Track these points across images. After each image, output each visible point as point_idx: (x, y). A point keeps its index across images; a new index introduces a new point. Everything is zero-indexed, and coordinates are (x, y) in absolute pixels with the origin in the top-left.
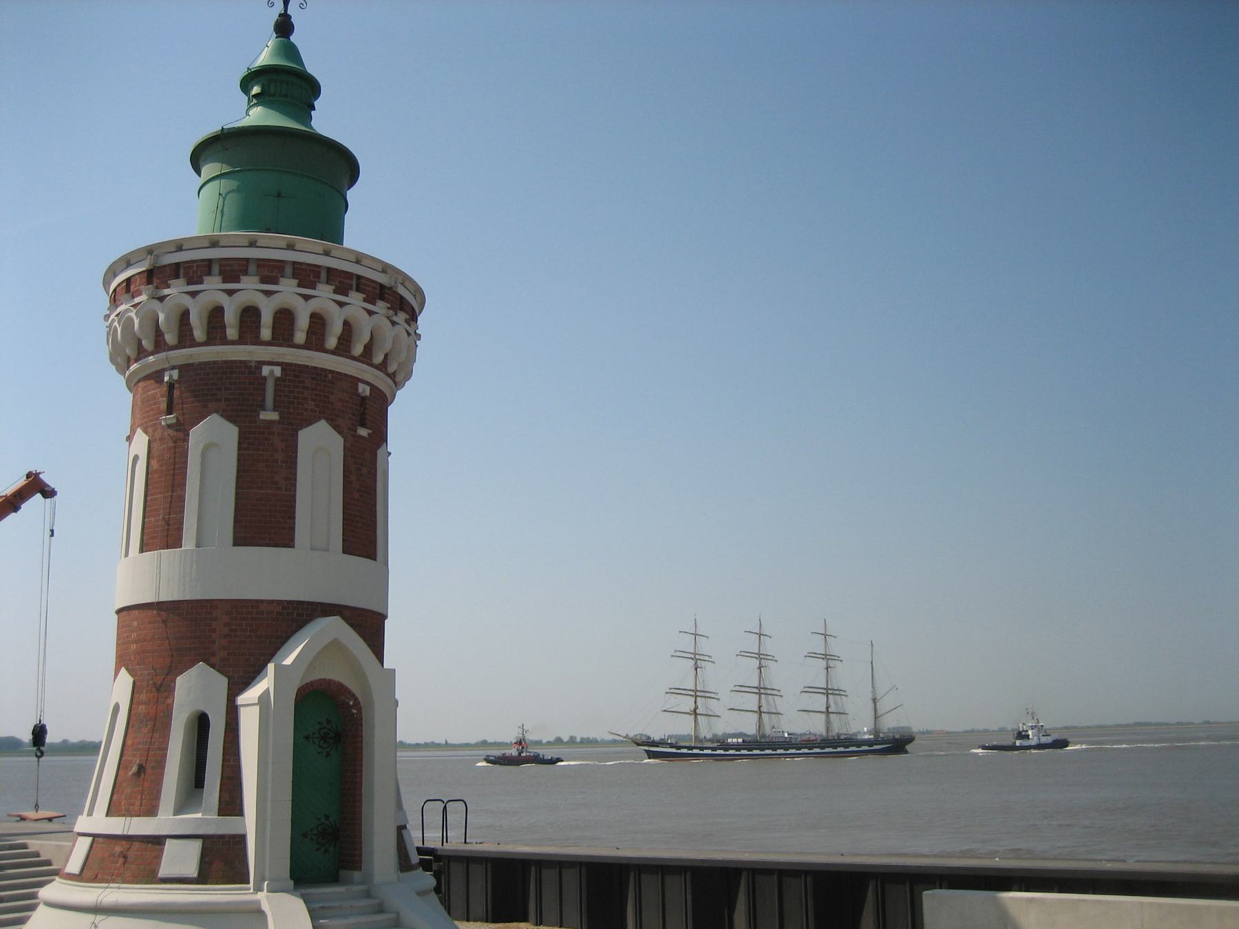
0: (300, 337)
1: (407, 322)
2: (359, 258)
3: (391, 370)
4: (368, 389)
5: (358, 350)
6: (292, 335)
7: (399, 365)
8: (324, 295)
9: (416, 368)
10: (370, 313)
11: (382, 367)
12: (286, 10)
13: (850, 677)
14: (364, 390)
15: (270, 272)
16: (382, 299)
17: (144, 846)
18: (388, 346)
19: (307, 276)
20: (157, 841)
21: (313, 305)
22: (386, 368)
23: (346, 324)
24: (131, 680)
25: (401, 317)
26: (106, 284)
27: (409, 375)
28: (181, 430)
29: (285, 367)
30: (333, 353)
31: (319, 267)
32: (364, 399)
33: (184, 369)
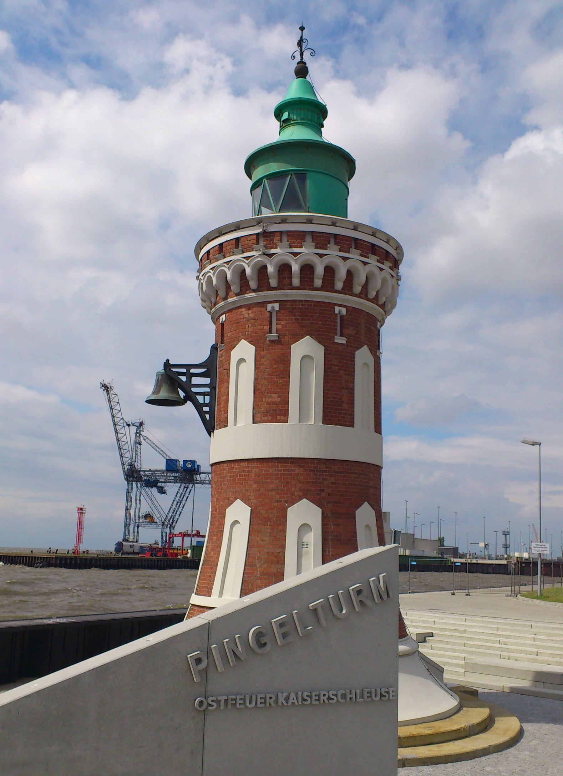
0: (318, 283)
2: (356, 227)
3: (381, 301)
5: (358, 289)
6: (312, 282)
9: (399, 301)
10: (365, 263)
11: (375, 300)
12: (302, 58)
13: (410, 525)
15: (297, 238)
19: (321, 240)
21: (326, 261)
23: (350, 273)
25: (386, 266)
26: (197, 255)
27: (394, 306)
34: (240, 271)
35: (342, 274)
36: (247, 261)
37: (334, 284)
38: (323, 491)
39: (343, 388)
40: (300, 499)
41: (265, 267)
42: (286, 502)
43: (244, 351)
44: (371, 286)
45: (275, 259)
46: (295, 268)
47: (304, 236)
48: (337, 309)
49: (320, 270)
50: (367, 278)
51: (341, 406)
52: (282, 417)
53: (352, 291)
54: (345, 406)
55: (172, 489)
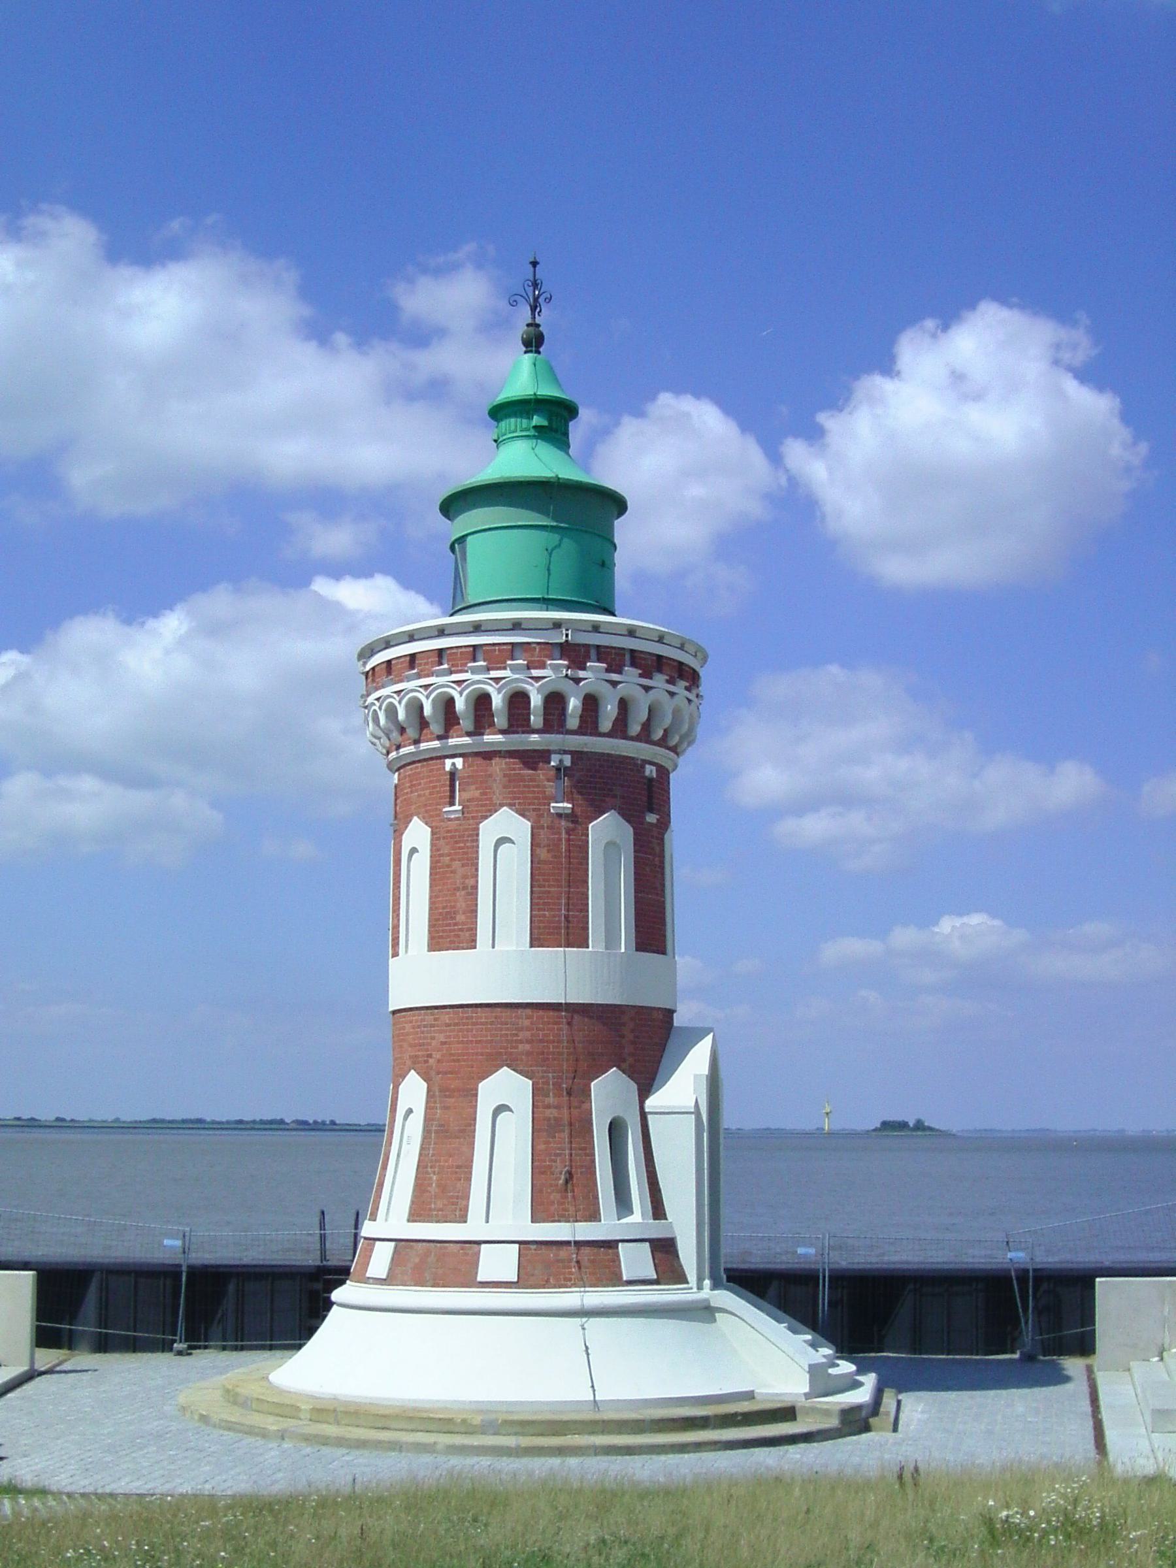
3: (672, 743)
4: (654, 768)
5: (635, 729)
8: (593, 674)
10: (647, 689)
11: (663, 743)
14: (650, 771)
16: (660, 671)
17: (596, 1250)
18: (667, 722)
20: (611, 1245)
23: (623, 705)
24: (424, 1085)
25: (680, 687)
28: (577, 822)
30: (608, 735)
31: (623, 649)
32: (651, 780)
33: (577, 755)
35: (610, 710)
36: (422, 690)
38: (430, 1056)
39: (457, 889)
46: (536, 700)
50: (650, 710)
51: (454, 918)
53: (625, 731)
54: (460, 918)
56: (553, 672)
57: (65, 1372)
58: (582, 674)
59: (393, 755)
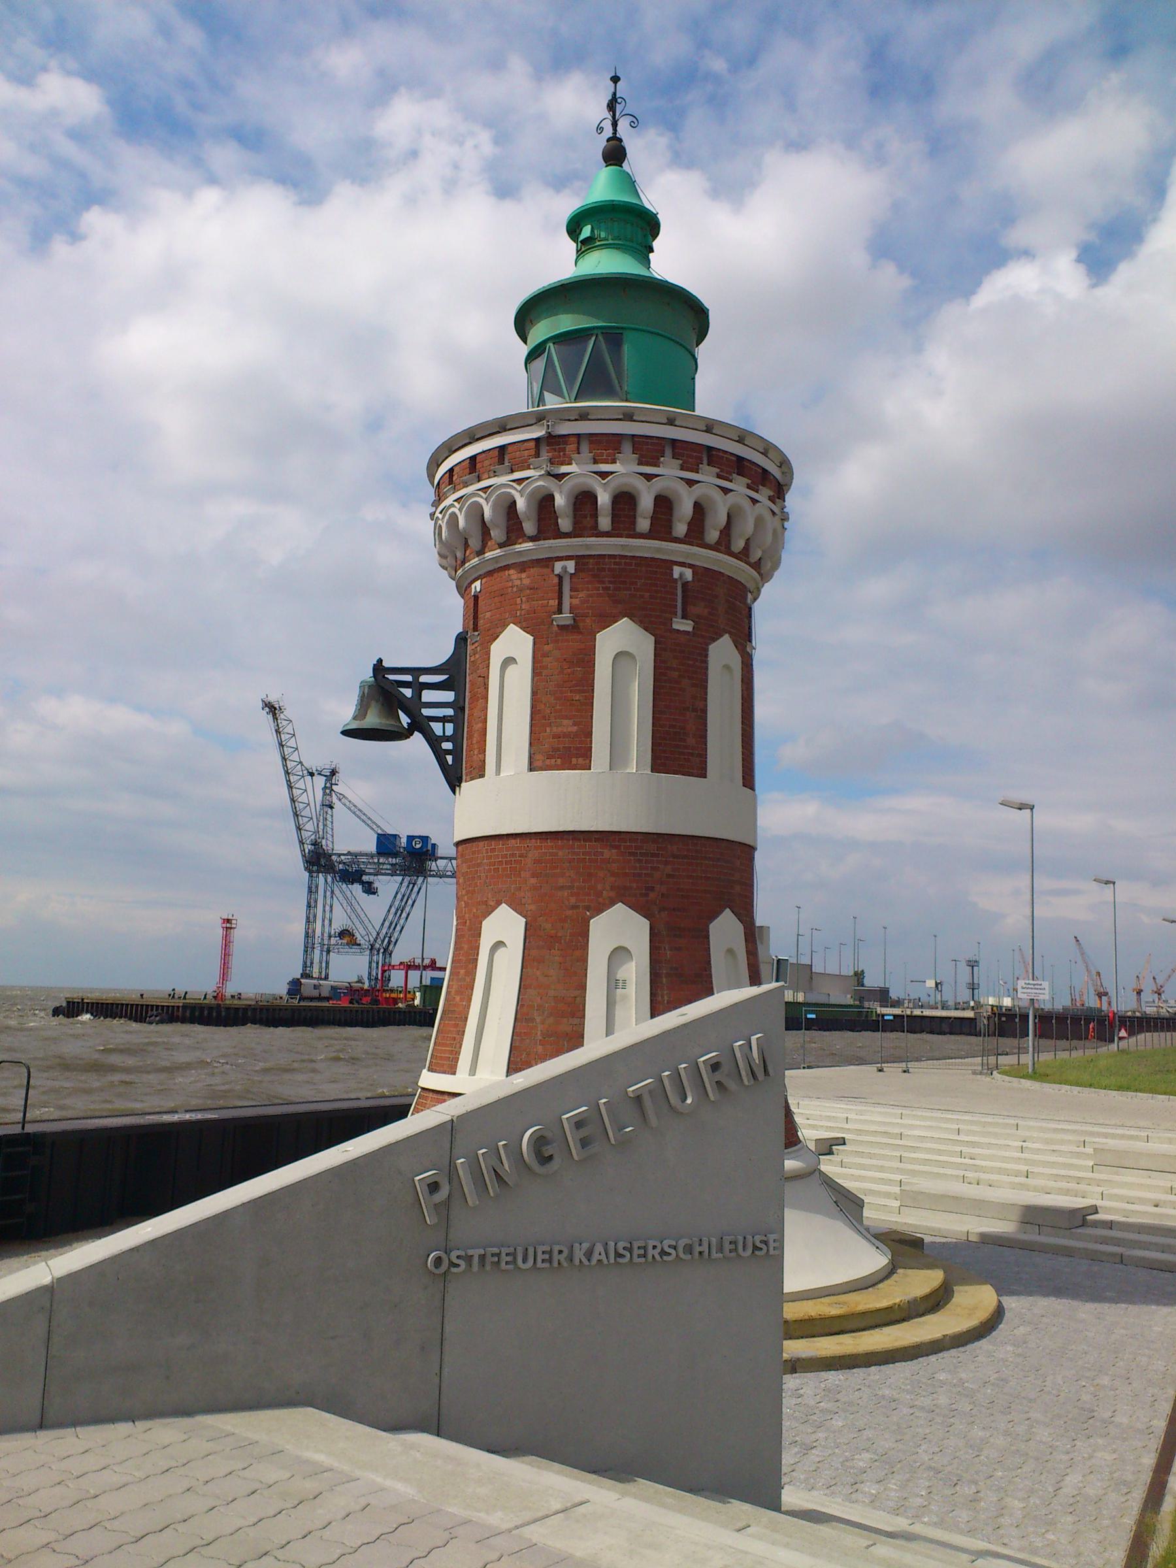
0: (643, 524)
1: (771, 499)
2: (710, 426)
5: (713, 535)
6: (634, 523)
7: (763, 551)
8: (669, 471)
10: (726, 491)
11: (743, 555)
13: (805, 948)
19: (649, 450)
21: (658, 485)
22: (748, 556)
23: (699, 508)
25: (763, 495)
26: (431, 476)
27: (776, 565)
29: (580, 560)
34: (507, 504)
35: (685, 509)
37: (671, 528)
40: (613, 903)
41: (550, 498)
42: (588, 908)
43: (514, 645)
44: (735, 532)
45: (568, 484)
46: (604, 498)
47: (620, 443)
48: (677, 571)
49: (646, 503)
52: (581, 761)
54: (691, 741)
55: (388, 885)
56: (624, 469)
57: (555, 1260)
58: (564, 469)
59: (460, 572)
